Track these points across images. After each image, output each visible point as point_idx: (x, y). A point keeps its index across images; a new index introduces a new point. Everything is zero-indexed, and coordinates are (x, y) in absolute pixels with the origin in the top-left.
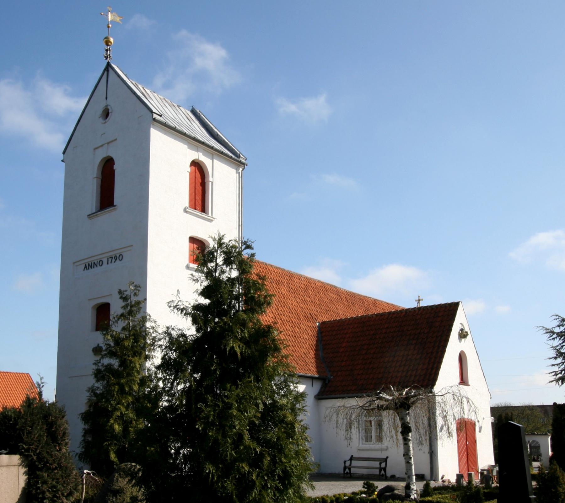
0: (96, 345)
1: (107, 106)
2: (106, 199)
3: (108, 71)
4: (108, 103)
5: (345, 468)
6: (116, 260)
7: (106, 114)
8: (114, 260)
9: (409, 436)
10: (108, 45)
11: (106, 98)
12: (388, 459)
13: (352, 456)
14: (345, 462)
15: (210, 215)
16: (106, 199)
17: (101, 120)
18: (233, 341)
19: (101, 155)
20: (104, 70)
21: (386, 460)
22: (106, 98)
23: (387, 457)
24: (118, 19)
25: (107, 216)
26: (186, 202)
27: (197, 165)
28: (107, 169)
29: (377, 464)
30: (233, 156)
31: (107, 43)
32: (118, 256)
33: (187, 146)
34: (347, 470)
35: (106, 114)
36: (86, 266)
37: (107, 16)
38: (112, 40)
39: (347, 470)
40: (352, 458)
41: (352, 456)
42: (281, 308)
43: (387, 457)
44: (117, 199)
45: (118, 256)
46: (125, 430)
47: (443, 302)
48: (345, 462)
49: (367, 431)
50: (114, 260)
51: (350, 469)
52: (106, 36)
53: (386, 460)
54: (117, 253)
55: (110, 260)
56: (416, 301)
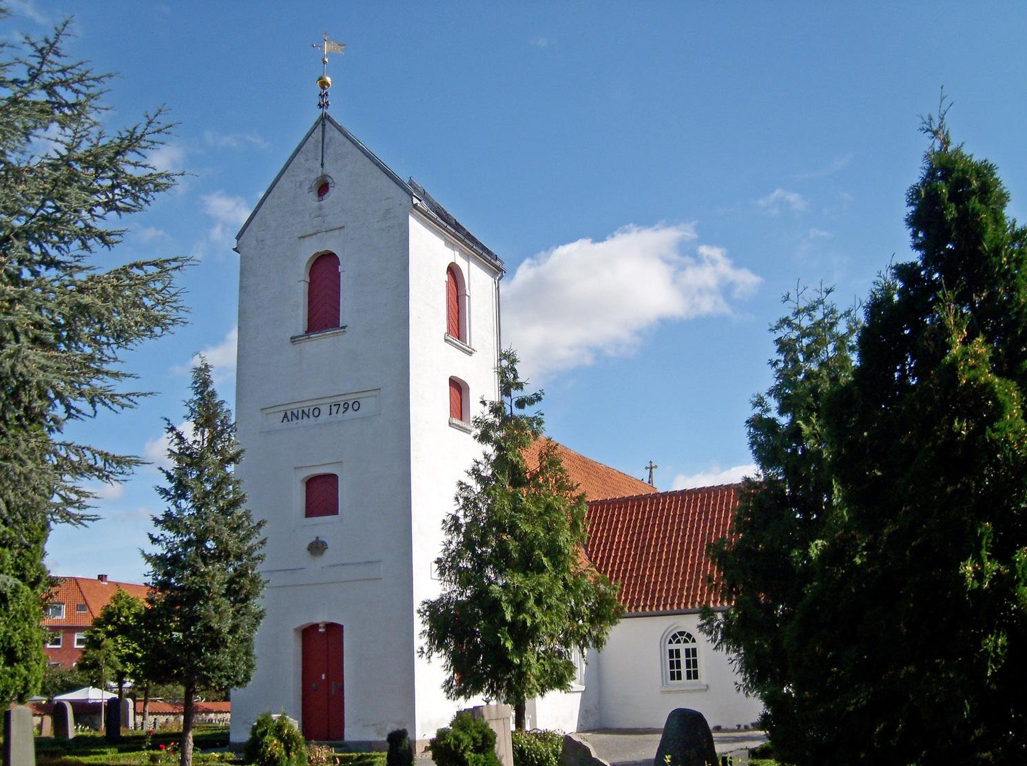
0: (314, 539)
1: (324, 176)
2: (323, 313)
3: (324, 125)
4: (325, 172)
6: (347, 408)
7: (323, 188)
8: (342, 409)
9: (901, 292)
10: (323, 88)
15: (468, 344)
16: (323, 313)
17: (314, 195)
19: (312, 248)
20: (317, 124)
24: (339, 50)
25: (323, 343)
26: (444, 328)
27: (453, 270)
28: (324, 270)
30: (435, 216)
31: (323, 84)
32: (351, 403)
33: (443, 242)
36: (286, 416)
37: (323, 47)
38: (329, 80)
44: (447, 345)
45: (351, 403)
46: (751, 515)
50: (342, 409)
52: (321, 74)
54: (350, 398)
55: (335, 409)
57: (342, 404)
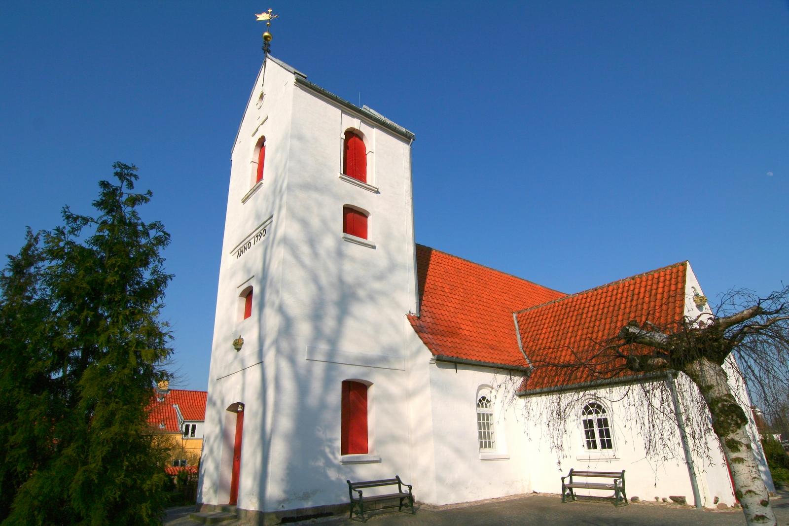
5: (564, 487)
11: (263, 85)
12: (625, 474)
13: (572, 470)
14: (563, 479)
18: (79, 357)
21: (622, 475)
22: (263, 85)
23: (624, 471)
27: (353, 140)
29: (610, 481)
34: (568, 491)
39: (568, 491)
40: (572, 473)
41: (572, 470)
42: (468, 280)
43: (624, 471)
47: (218, 297)
48: (563, 479)
49: (590, 434)
51: (571, 489)
53: (622, 475)
56: (164, 260)
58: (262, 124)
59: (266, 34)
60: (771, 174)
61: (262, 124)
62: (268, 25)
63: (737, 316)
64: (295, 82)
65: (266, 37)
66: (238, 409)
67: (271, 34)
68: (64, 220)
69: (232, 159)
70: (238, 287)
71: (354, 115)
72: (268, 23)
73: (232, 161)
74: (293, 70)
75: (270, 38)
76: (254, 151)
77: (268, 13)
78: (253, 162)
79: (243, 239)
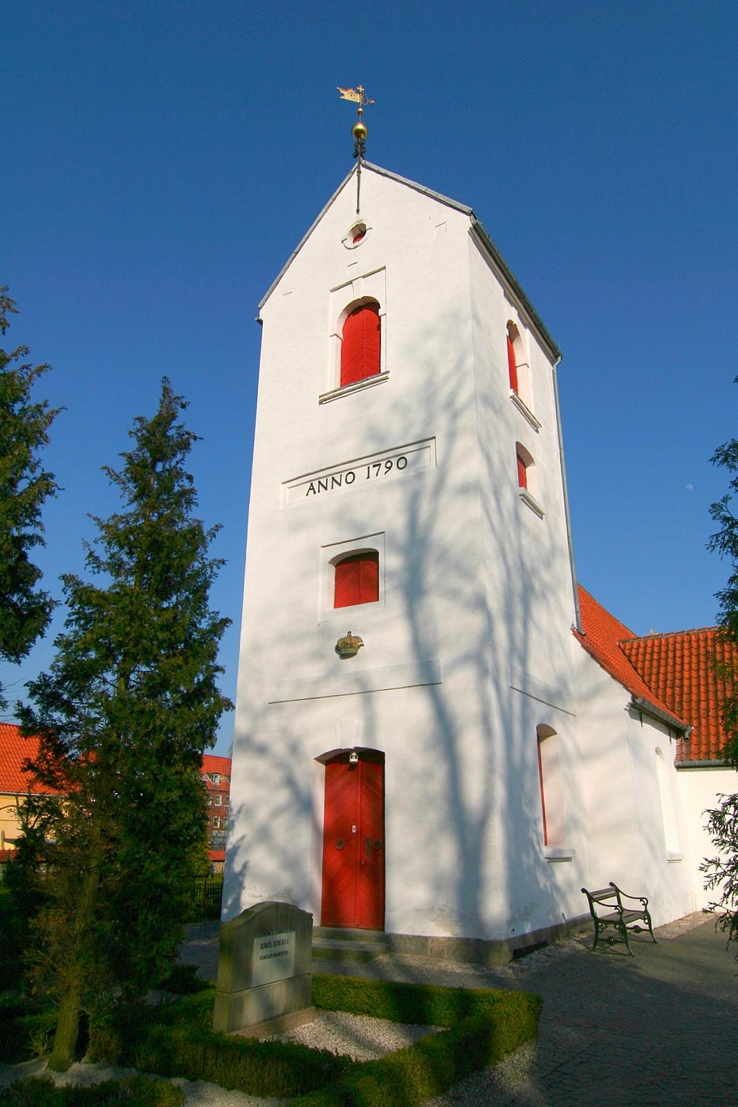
7: (359, 232)
22: (358, 211)
35: (359, 232)
36: (312, 488)
57: (383, 463)
58: (364, 277)
59: (360, 126)
60: (690, 487)
61: (364, 277)
62: (359, 112)
63: (69, 601)
64: (470, 229)
65: (358, 133)
66: (358, 771)
67: (368, 131)
68: (731, 472)
69: (263, 314)
70: (323, 547)
71: (514, 302)
72: (360, 110)
73: (261, 322)
74: (467, 209)
75: (364, 134)
76: (340, 317)
77: (358, 92)
78: (336, 335)
79: (331, 466)
